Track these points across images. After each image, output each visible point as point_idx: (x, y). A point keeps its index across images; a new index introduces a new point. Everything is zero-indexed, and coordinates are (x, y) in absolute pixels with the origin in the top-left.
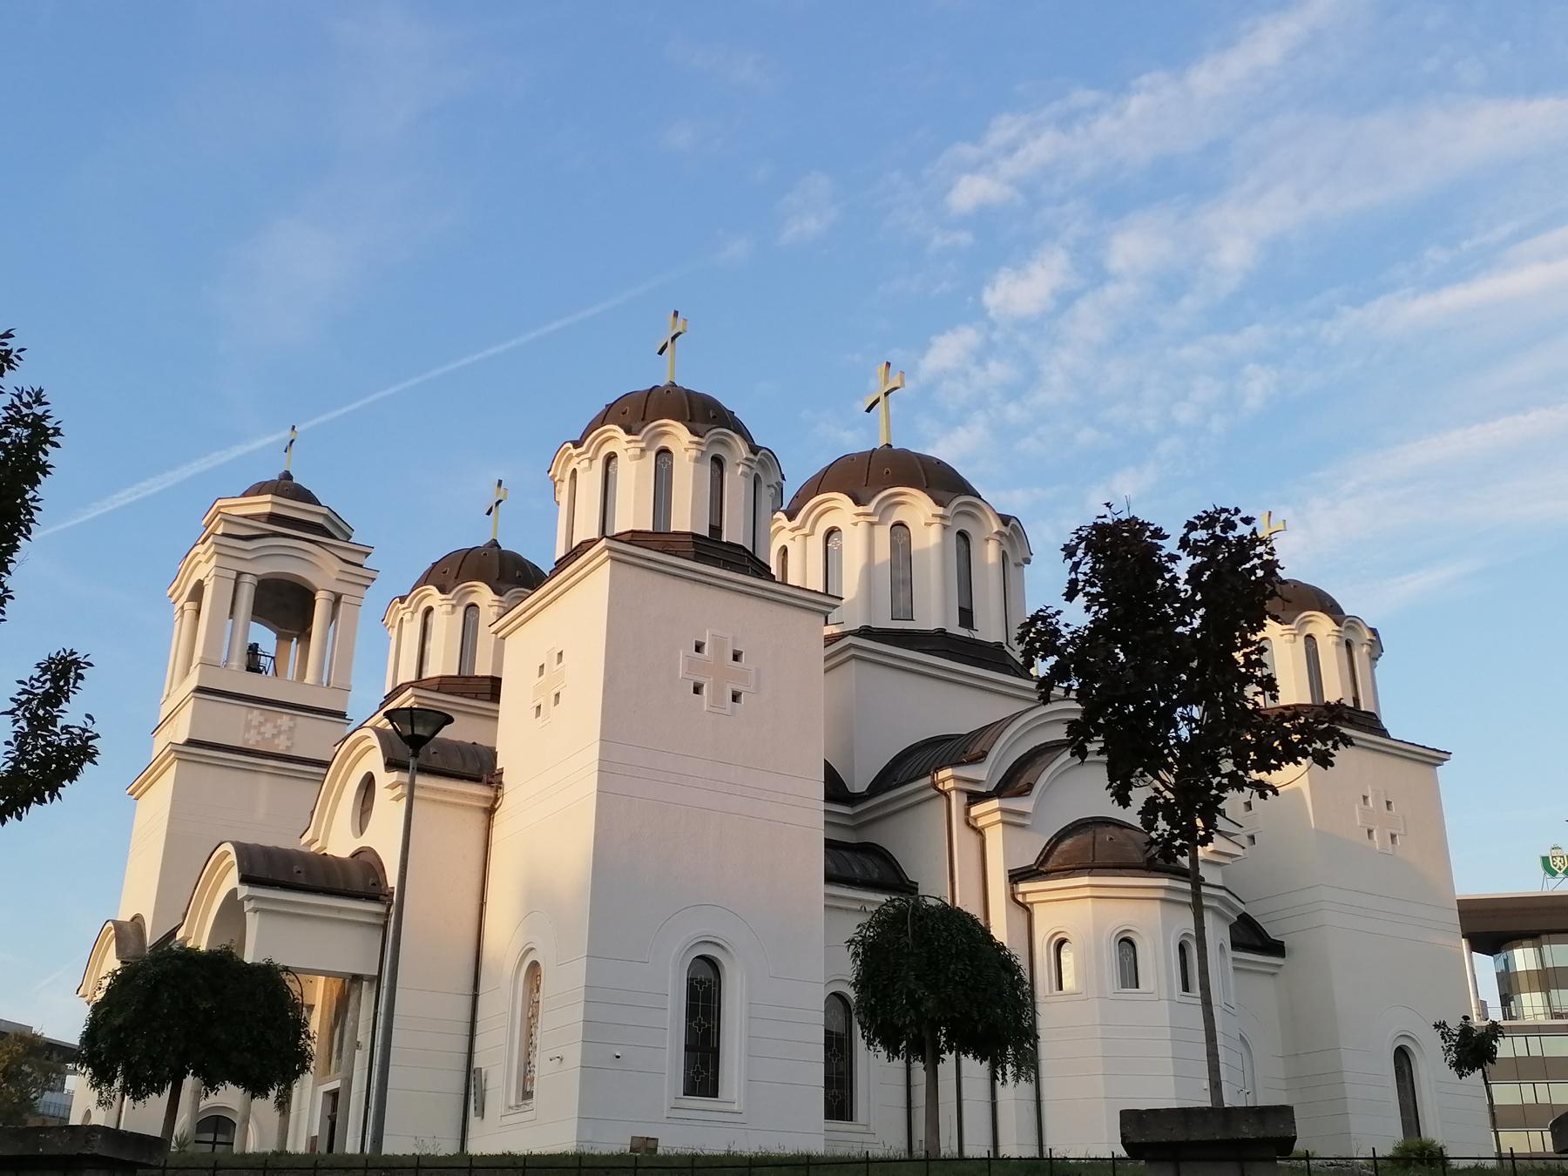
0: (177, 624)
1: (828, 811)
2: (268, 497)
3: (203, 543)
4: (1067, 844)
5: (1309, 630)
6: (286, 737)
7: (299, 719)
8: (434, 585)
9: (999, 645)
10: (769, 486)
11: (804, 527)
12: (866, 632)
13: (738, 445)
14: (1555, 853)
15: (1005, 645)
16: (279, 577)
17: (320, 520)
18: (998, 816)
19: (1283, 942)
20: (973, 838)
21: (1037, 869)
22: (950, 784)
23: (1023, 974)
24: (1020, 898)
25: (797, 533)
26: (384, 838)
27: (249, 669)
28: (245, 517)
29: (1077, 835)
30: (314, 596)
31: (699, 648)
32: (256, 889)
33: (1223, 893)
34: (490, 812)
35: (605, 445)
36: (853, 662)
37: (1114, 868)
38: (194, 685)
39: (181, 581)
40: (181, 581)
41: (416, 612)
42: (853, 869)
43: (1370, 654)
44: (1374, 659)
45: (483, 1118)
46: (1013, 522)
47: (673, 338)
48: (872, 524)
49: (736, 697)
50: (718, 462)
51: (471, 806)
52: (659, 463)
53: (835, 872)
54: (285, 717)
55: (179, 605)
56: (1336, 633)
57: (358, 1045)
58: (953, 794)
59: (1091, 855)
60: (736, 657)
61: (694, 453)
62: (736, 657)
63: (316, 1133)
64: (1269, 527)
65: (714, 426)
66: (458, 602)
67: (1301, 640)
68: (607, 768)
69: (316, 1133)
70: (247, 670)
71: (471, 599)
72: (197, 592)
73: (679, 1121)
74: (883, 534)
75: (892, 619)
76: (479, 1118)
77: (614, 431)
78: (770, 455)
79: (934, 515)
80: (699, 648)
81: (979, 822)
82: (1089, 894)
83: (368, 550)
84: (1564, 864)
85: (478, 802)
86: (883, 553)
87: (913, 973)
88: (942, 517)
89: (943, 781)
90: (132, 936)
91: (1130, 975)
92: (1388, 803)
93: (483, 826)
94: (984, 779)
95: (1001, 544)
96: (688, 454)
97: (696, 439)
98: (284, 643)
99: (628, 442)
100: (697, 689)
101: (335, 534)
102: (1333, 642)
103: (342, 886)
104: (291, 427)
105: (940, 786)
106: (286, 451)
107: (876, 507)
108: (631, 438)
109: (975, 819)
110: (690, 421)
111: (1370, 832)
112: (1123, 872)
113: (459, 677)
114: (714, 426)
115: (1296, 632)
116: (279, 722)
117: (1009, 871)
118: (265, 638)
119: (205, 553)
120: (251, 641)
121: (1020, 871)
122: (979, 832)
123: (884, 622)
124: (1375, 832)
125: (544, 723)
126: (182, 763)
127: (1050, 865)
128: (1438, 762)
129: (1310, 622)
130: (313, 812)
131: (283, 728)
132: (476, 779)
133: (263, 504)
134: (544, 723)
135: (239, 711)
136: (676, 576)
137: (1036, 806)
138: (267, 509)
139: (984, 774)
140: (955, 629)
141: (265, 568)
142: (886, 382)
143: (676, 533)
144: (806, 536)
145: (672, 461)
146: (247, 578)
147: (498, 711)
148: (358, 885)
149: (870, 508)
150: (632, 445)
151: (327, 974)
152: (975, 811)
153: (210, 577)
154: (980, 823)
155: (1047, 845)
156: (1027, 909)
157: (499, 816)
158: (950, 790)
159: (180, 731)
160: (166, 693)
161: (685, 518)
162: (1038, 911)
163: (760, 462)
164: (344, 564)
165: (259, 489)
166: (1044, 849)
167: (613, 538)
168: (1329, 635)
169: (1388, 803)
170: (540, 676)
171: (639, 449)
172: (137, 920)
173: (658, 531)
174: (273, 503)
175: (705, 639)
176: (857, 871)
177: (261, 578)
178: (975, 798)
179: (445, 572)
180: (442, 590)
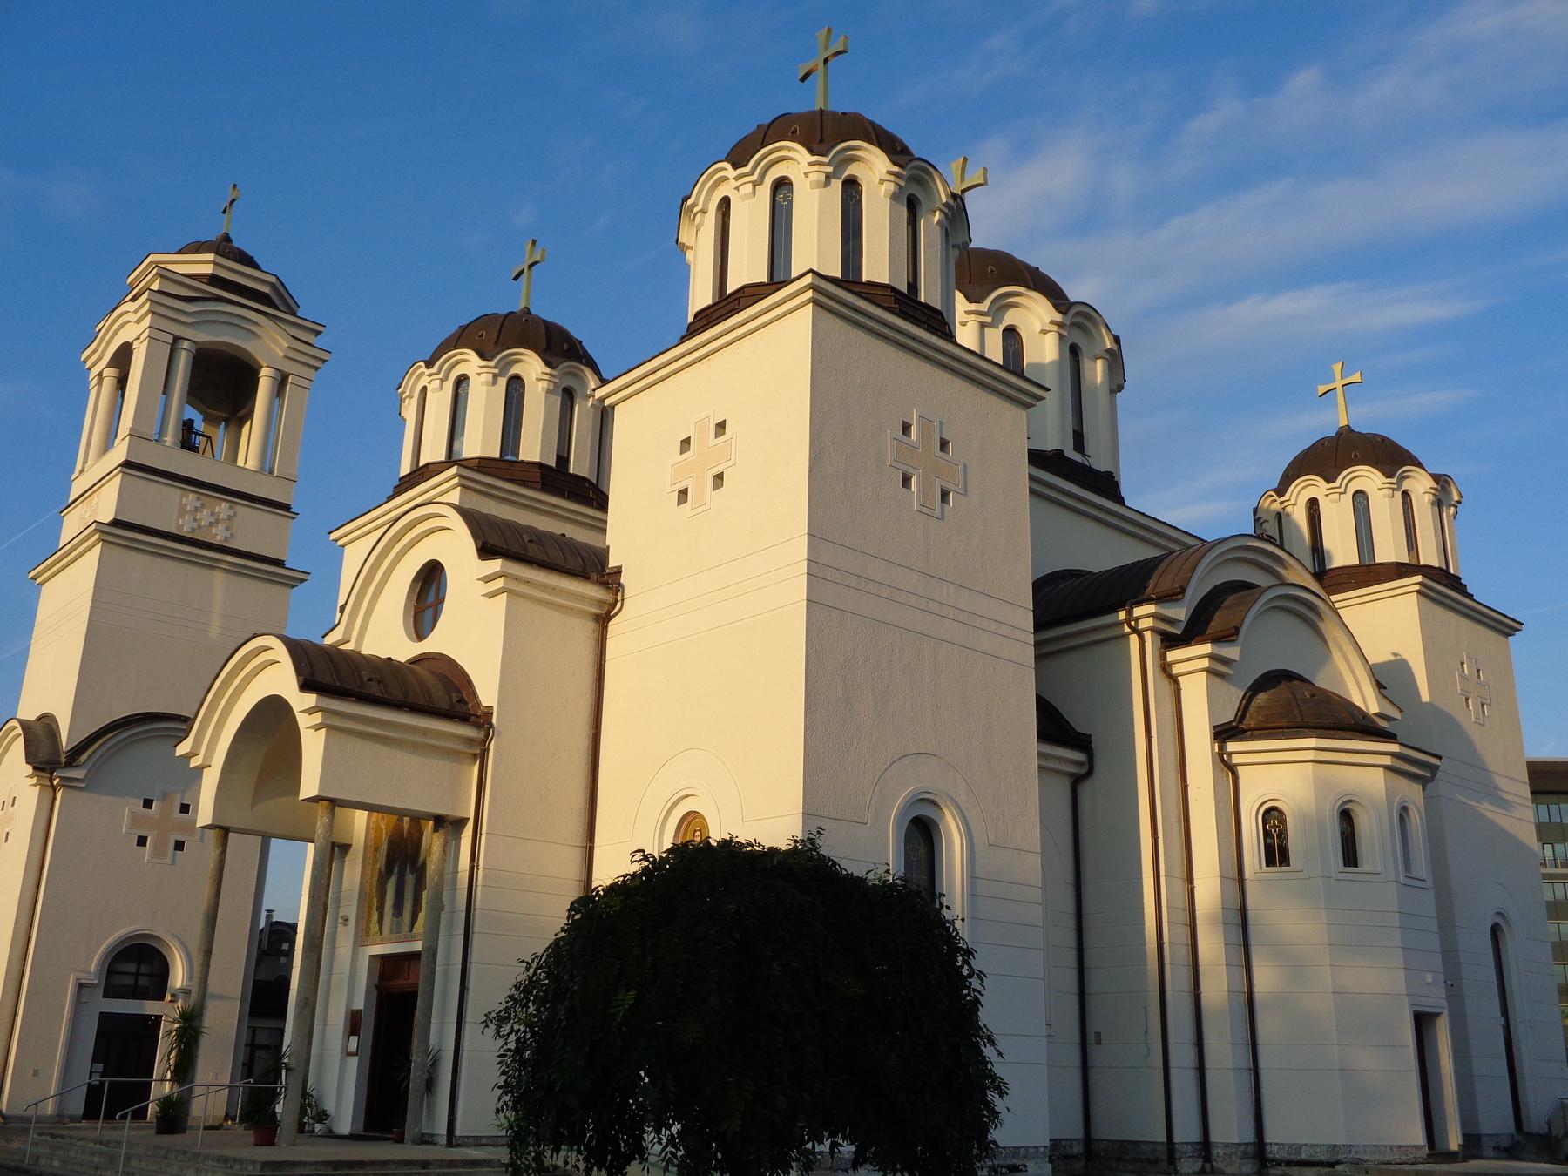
2: (211, 257)
3: (134, 299)
6: (225, 525)
7: (239, 509)
8: (472, 349)
17: (266, 289)
22: (1143, 624)
34: (603, 620)
38: (123, 458)
39: (99, 345)
40: (99, 345)
41: (446, 380)
48: (983, 325)
51: (581, 611)
54: (223, 504)
58: (1148, 635)
60: (944, 445)
62: (944, 445)
63: (359, 1004)
66: (500, 372)
67: (1398, 495)
69: (359, 1004)
70: (183, 447)
71: (515, 370)
72: (123, 357)
77: (789, 149)
79: (1052, 322)
82: (1311, 758)
83: (319, 328)
90: (44, 739)
97: (896, 169)
99: (811, 164)
102: (1429, 500)
106: (224, 212)
107: (991, 304)
108: (816, 158)
113: (500, 460)
115: (1395, 486)
116: (217, 509)
117: (1214, 727)
119: (136, 312)
120: (186, 418)
121: (1224, 728)
122: (1174, 680)
125: (694, 512)
129: (1408, 477)
131: (221, 516)
133: (203, 264)
134: (694, 512)
138: (208, 269)
141: (202, 337)
142: (962, 180)
146: (186, 345)
148: (440, 698)
149: (984, 306)
150: (816, 168)
153: (142, 339)
155: (1243, 699)
156: (1232, 769)
157: (614, 627)
159: (105, 507)
160: (79, 467)
164: (294, 341)
165: (198, 248)
172: (47, 721)
174: (214, 263)
175: (912, 419)
178: (1169, 641)
179: (482, 336)
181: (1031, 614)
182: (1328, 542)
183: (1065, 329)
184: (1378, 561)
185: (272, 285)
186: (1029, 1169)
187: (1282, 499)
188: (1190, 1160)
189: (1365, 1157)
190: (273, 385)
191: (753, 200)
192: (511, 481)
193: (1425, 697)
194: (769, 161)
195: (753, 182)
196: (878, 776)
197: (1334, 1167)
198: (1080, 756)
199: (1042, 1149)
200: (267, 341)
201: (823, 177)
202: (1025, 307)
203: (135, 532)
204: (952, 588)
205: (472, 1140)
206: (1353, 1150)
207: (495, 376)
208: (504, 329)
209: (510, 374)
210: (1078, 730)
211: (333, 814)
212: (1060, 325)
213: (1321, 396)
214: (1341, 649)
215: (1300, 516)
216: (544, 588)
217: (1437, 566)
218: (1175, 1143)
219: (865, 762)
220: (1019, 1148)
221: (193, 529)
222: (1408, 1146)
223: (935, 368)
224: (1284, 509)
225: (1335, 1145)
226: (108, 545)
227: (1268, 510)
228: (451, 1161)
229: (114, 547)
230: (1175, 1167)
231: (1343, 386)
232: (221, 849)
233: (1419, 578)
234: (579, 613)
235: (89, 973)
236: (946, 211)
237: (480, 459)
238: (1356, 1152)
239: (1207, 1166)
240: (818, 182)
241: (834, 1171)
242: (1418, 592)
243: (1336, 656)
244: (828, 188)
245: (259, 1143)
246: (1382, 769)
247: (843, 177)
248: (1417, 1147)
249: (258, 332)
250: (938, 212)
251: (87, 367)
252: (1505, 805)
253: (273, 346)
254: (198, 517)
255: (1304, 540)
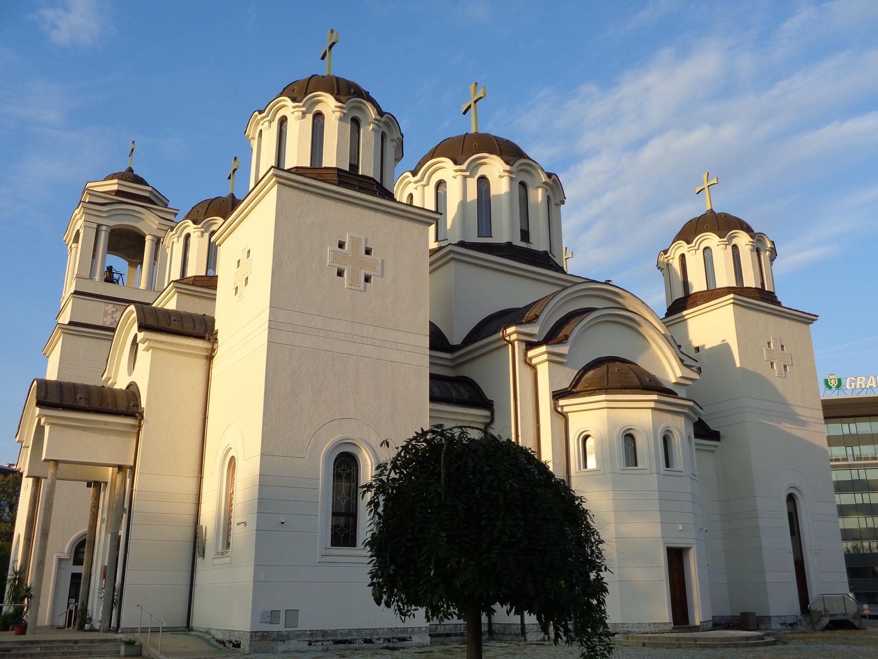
0: (69, 256)
1: (207, 287)
2: (116, 181)
4: (590, 373)
5: (734, 242)
9: (546, 253)
10: (392, 140)
11: (423, 180)
12: (462, 244)
13: (369, 109)
14: (831, 377)
15: (549, 253)
16: (130, 229)
17: (147, 194)
18: (545, 357)
19: (719, 432)
20: (529, 371)
21: (571, 390)
23: (591, 522)
24: (559, 409)
25: (418, 184)
26: (141, 377)
27: (106, 280)
28: (104, 192)
29: (596, 368)
30: (145, 238)
31: (341, 245)
32: (45, 410)
33: (691, 404)
34: (210, 358)
35: (280, 111)
36: (452, 263)
37: (621, 388)
42: (451, 393)
43: (770, 257)
44: (772, 260)
45: (204, 558)
46: (554, 177)
47: (330, 47)
48: (465, 177)
49: (367, 279)
50: (356, 122)
51: (197, 355)
52: (315, 122)
53: (439, 395)
55: (69, 246)
56: (751, 243)
57: (124, 510)
58: (516, 343)
59: (606, 380)
60: (368, 252)
61: (338, 114)
62: (368, 252)
64: (708, 182)
65: (350, 97)
67: (730, 248)
68: (274, 326)
73: (328, 564)
74: (472, 183)
75: (478, 237)
76: (202, 558)
77: (285, 101)
78: (393, 119)
79: (505, 171)
80: (341, 245)
81: (533, 361)
84: (836, 383)
85: (201, 352)
86: (473, 195)
87: (444, 535)
88: (509, 172)
89: (510, 335)
91: (632, 457)
92: (782, 346)
93: (206, 367)
94: (537, 333)
95: (546, 190)
96: (334, 115)
97: (340, 104)
98: (133, 269)
100: (340, 273)
101: (157, 203)
102: (749, 249)
103: (110, 407)
104: (132, 142)
105: (507, 338)
109: (531, 359)
110: (337, 94)
111: (772, 364)
112: (627, 391)
114: (350, 97)
115: (727, 243)
117: (553, 392)
118: (119, 264)
121: (560, 392)
122: (534, 368)
123: (474, 238)
124: (774, 364)
126: (66, 335)
127: (579, 388)
128: (811, 322)
130: (107, 360)
132: (201, 337)
133: (113, 185)
134: (240, 298)
135: (100, 305)
136: (325, 196)
137: (570, 351)
138: (115, 187)
139: (535, 330)
140: (518, 242)
141: (113, 223)
143: (326, 168)
144: (424, 186)
145: (324, 121)
146: (104, 228)
147: (215, 295)
148: (122, 406)
149: (464, 167)
150: (297, 109)
151: (113, 466)
152: (530, 354)
154: (534, 361)
156: (564, 416)
158: (514, 341)
159: (65, 319)
161: (330, 160)
162: (570, 416)
163: (385, 123)
164: (162, 220)
166: (575, 377)
167: (289, 171)
168: (746, 245)
169: (782, 346)
170: (238, 267)
171: (301, 113)
173: (315, 167)
176: (454, 394)
177: (112, 229)
178: (530, 345)
179: (198, 212)
180: (195, 222)
181: (428, 338)
182: (690, 279)
183: (514, 174)
184: (718, 287)
185: (151, 192)
186: (414, 639)
187: (666, 256)
188: (535, 633)
189: (633, 630)
190: (152, 244)
191: (269, 130)
192: (202, 286)
193: (738, 365)
194: (278, 107)
195: (268, 120)
196: (313, 432)
197: (614, 636)
198: (487, 413)
199: (424, 629)
200: (148, 222)
201: (300, 114)
202: (490, 164)
203: (79, 327)
204: (371, 328)
205: (130, 630)
206: (626, 626)
207: (202, 233)
208: (210, 207)
209: (211, 230)
210: (489, 398)
211: (57, 468)
212: (509, 172)
213: (698, 193)
214: (655, 342)
215: (676, 264)
216: (173, 344)
217: (754, 286)
218: (525, 624)
219: (305, 425)
220: (407, 628)
221: (112, 323)
222: (660, 623)
223: (356, 208)
224: (668, 261)
225: (615, 623)
226: (67, 335)
227: (663, 262)
228: (92, 640)
229: (69, 335)
230: (525, 638)
231: (708, 186)
232: (35, 488)
233: (732, 296)
234: (196, 356)
235: (64, 553)
236: (377, 122)
237: (195, 276)
238: (627, 627)
239: (546, 636)
240: (298, 116)
241: (275, 641)
242: (733, 303)
243: (653, 345)
244: (304, 119)
245: (17, 634)
246: (650, 410)
247: (313, 112)
248: (665, 624)
249: (142, 217)
250: (372, 124)
251: (66, 243)
252: (802, 423)
253: (152, 224)
254: (114, 316)
255: (679, 278)
